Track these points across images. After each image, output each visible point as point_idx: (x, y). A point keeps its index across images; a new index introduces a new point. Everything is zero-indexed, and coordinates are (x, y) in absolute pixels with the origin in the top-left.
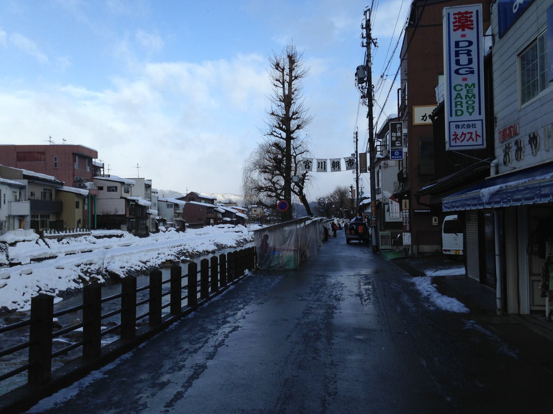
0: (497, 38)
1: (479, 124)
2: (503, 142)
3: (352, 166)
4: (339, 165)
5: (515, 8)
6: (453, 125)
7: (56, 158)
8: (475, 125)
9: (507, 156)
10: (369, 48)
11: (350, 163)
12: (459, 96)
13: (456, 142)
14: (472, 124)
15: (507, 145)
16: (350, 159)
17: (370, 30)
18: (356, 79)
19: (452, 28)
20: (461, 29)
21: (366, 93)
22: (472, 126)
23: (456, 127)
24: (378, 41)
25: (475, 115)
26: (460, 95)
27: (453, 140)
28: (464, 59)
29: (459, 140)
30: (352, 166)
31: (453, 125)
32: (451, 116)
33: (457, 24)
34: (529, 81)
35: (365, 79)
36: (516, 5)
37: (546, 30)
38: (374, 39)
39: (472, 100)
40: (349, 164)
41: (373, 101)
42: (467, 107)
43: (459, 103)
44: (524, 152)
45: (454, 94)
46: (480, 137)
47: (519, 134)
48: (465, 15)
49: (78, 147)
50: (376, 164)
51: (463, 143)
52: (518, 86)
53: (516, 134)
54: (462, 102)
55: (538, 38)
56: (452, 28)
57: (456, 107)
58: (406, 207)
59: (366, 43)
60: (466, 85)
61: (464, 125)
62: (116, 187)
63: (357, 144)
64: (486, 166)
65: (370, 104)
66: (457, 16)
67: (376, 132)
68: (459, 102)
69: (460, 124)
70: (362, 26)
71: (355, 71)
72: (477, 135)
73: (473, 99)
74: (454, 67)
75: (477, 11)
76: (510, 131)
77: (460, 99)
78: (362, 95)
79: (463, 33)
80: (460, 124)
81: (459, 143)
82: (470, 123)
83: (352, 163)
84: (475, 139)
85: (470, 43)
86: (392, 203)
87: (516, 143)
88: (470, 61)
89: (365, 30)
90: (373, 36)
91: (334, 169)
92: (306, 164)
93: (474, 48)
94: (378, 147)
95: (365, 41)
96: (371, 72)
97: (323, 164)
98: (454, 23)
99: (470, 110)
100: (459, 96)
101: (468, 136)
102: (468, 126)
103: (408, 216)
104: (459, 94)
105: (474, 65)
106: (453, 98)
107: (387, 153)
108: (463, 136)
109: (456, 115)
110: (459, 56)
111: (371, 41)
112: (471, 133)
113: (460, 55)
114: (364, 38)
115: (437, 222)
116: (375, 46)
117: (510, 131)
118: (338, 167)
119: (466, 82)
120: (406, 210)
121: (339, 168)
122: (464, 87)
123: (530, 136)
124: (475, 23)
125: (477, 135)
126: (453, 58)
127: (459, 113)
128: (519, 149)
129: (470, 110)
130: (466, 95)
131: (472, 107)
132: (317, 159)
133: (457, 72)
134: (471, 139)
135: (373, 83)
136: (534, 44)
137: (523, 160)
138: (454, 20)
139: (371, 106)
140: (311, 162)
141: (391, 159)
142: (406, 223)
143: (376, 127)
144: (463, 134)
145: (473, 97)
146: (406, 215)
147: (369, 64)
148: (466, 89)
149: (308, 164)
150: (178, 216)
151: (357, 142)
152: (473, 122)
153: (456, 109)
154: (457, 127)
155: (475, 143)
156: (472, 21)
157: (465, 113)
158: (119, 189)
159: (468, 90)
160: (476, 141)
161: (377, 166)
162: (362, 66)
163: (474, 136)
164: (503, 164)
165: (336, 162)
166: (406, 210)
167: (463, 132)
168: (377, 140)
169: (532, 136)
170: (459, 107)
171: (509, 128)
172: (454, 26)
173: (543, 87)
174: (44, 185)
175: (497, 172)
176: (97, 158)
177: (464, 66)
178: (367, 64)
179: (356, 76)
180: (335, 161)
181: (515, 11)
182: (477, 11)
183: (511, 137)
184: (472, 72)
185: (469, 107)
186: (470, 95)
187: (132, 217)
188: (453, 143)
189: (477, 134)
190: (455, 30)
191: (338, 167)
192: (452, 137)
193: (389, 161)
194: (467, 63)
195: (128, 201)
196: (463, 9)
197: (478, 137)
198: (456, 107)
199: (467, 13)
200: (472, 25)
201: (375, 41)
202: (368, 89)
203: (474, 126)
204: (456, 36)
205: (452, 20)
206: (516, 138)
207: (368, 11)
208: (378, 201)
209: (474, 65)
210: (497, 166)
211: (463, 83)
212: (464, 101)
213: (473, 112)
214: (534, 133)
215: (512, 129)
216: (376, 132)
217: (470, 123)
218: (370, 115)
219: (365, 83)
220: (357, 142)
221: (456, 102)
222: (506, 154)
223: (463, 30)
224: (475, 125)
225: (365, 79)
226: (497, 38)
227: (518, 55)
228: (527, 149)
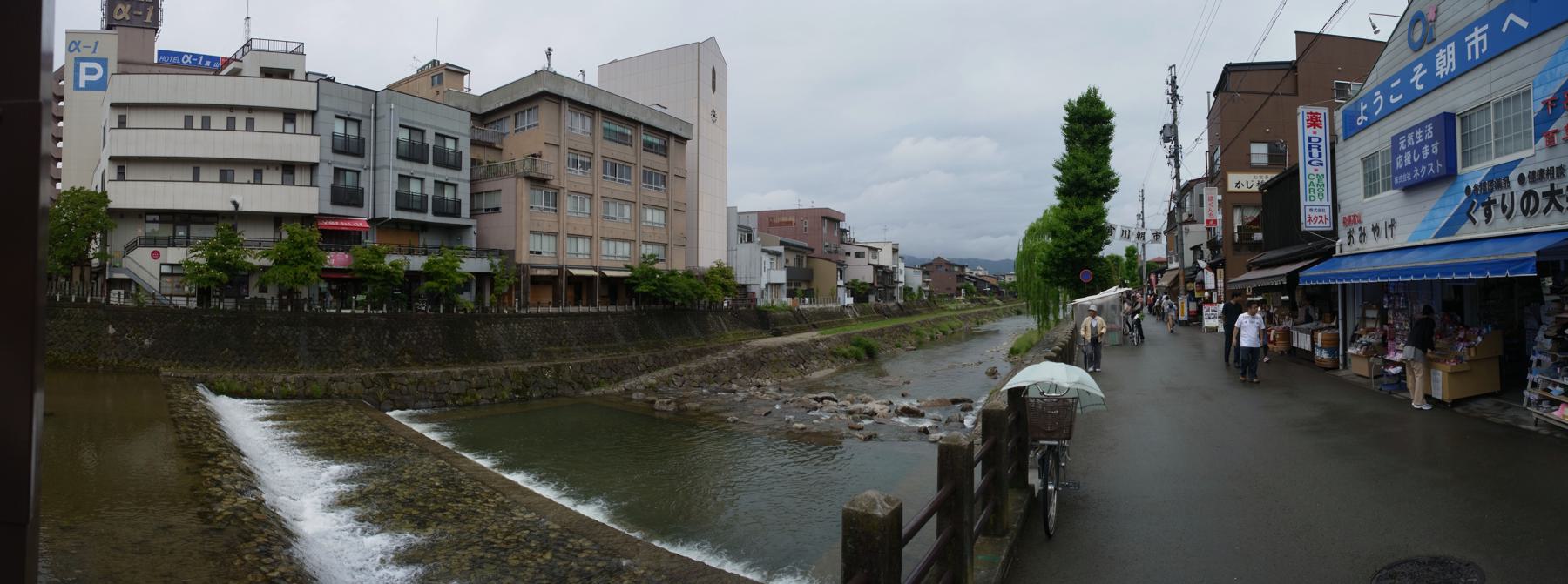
1: (1327, 209)
19: (1306, 125)
25: (1325, 202)
28: (1315, 152)
45: (1308, 181)
53: (1360, 222)
62: (864, 253)
69: (1314, 208)
74: (1308, 159)
80: (1314, 208)
81: (1312, 224)
82: (1321, 208)
85: (1320, 140)
87: (1360, 228)
88: (1320, 155)
93: (1322, 144)
101: (1319, 219)
102: (1320, 210)
105: (1323, 159)
124: (1323, 123)
127: (1312, 198)
128: (1363, 235)
139: (1178, 167)
150: (926, 286)
154: (1311, 210)
157: (1317, 200)
158: (866, 254)
163: (1324, 219)
174: (796, 251)
175: (1341, 251)
177: (1315, 159)
181: (1359, 124)
183: (1355, 223)
184: (1322, 165)
187: (879, 285)
188: (1308, 224)
190: (1308, 127)
192: (1307, 219)
195: (877, 267)
196: (1314, 110)
199: (1317, 114)
203: (1323, 210)
204: (1309, 132)
205: (1306, 118)
209: (1323, 159)
210: (1341, 245)
211: (1315, 173)
212: (1316, 188)
217: (1321, 208)
222: (1350, 236)
228: (1370, 234)
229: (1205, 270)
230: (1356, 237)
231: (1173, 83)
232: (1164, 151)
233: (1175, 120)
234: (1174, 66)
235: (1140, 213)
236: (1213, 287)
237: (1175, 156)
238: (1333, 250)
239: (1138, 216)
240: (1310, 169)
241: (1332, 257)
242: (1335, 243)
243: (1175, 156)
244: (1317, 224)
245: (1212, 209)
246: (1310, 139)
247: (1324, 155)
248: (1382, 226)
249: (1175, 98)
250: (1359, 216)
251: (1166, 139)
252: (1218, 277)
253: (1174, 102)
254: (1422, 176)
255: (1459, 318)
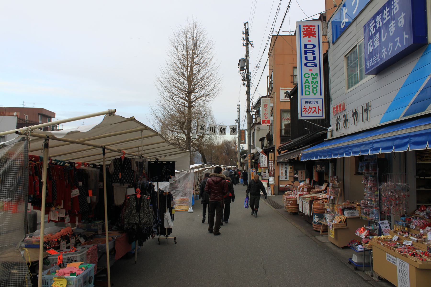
0: (331, 44)
1: (320, 102)
2: (336, 115)
3: (234, 132)
4: (225, 131)
5: (343, 25)
6: (303, 101)
7: (27, 117)
8: (318, 102)
9: (338, 124)
10: (247, 48)
11: (233, 130)
12: (307, 81)
13: (305, 114)
14: (316, 101)
15: (338, 117)
16: (233, 127)
17: (248, 35)
18: (239, 68)
19: (302, 35)
20: (308, 36)
21: (245, 77)
22: (316, 103)
23: (305, 103)
24: (253, 43)
25: (318, 96)
26: (308, 81)
27: (303, 112)
28: (310, 56)
29: (307, 112)
30: (234, 132)
31: (303, 101)
32: (302, 95)
33: (305, 33)
34: (352, 74)
35: (245, 68)
36: (343, 23)
37: (363, 40)
38: (251, 42)
39: (316, 85)
40: (233, 131)
41: (251, 84)
42: (313, 89)
43: (308, 86)
44: (349, 122)
45: (304, 79)
46: (321, 110)
47: (346, 110)
48: (310, 27)
49: (42, 109)
50: (252, 128)
51: (309, 115)
52: (345, 76)
53: (344, 110)
54: (309, 86)
55: (358, 45)
56: (302, 35)
57: (305, 89)
58: (271, 159)
59: (246, 44)
60: (312, 74)
61: (311, 101)
63: (239, 113)
64: (325, 131)
65: (248, 85)
66: (305, 28)
67: (252, 105)
68: (307, 85)
69: (308, 101)
70: (243, 32)
71: (238, 62)
72: (319, 109)
73: (316, 84)
74: (304, 61)
75: (318, 26)
76: (340, 108)
77: (308, 83)
78: (243, 78)
79: (310, 39)
80: (308, 101)
81: (307, 114)
82: (315, 100)
83: (234, 130)
84: (317, 112)
85: (314, 46)
86: (262, 156)
87: (344, 116)
88: (314, 58)
89: (245, 35)
90: (250, 40)
91: (221, 133)
92: (201, 127)
93: (316, 49)
94: (253, 115)
95: (245, 42)
96: (249, 63)
97: (214, 128)
98: (303, 32)
99: (315, 92)
100: (307, 81)
101: (313, 109)
102: (314, 103)
103: (272, 165)
104: (307, 80)
105: (317, 61)
106: (303, 83)
107: (260, 120)
108: (310, 109)
109: (306, 95)
110: (307, 54)
111: (249, 43)
112: (315, 108)
113: (308, 54)
114: (245, 40)
115: (292, 170)
116: (252, 46)
117: (340, 108)
118: (224, 132)
119: (311, 72)
120: (271, 161)
121: (225, 133)
122: (310, 75)
123: (353, 111)
125: (319, 109)
126: (303, 56)
127: (307, 93)
128: (346, 121)
129: (315, 92)
130: (312, 81)
131: (315, 89)
132: (229, 126)
133: (306, 64)
134: (315, 112)
135: (251, 70)
136: (355, 50)
137: (348, 128)
138: (304, 30)
139: (248, 86)
140: (205, 126)
141: (262, 124)
142: (271, 170)
143: (252, 101)
144: (310, 108)
145: (316, 83)
146: (271, 164)
147: (248, 58)
148: (312, 77)
149: (203, 127)
151: (239, 111)
152: (317, 100)
153: (305, 90)
154: (306, 102)
155: (317, 115)
156: (315, 32)
159: (313, 78)
160: (319, 113)
161: (252, 129)
162: (243, 59)
163: (317, 110)
164: (336, 130)
165: (223, 128)
166: (271, 161)
167: (310, 107)
168: (253, 110)
169: (354, 111)
170: (307, 89)
171: (340, 105)
172: (304, 34)
173: (361, 79)
175: (332, 136)
176: (55, 117)
177: (310, 61)
178: (246, 58)
179: (238, 65)
180: (223, 127)
182: (318, 26)
184: (316, 66)
185: (314, 89)
186: (315, 81)
188: (303, 114)
189: (319, 108)
190: (304, 37)
191: (224, 132)
192: (303, 110)
193: (261, 126)
194: (312, 59)
197: (319, 110)
198: (305, 89)
199: (311, 26)
200: (315, 34)
201: (251, 43)
202: (247, 75)
203: (317, 103)
205: (302, 30)
206: (344, 113)
207: (247, 23)
208: (253, 154)
209: (317, 61)
210: (332, 131)
211: (310, 73)
212: (311, 85)
213: (316, 93)
214: (356, 109)
215: (341, 106)
216: (252, 105)
217: (315, 100)
218: (248, 93)
219: (245, 70)
220: (239, 111)
221: (305, 86)
223: (309, 37)
224: (318, 102)
225: (245, 68)
226: (331, 44)
227: (345, 56)
228: (351, 119)
229: (261, 154)
230: (341, 123)
231: (247, 33)
232: (238, 76)
233: (247, 56)
234: (248, 22)
235: (237, 119)
236: (266, 165)
237: (247, 79)
238: (325, 135)
239: (236, 120)
240: (306, 70)
241: (324, 141)
242: (327, 130)
243: (247, 79)
244: (311, 114)
245: (266, 112)
246: (306, 46)
247: (317, 58)
248: (360, 111)
249: (248, 43)
250: (343, 105)
251: (242, 69)
252: (270, 159)
253: (247, 45)
254: (389, 54)
255: (112, 254)
